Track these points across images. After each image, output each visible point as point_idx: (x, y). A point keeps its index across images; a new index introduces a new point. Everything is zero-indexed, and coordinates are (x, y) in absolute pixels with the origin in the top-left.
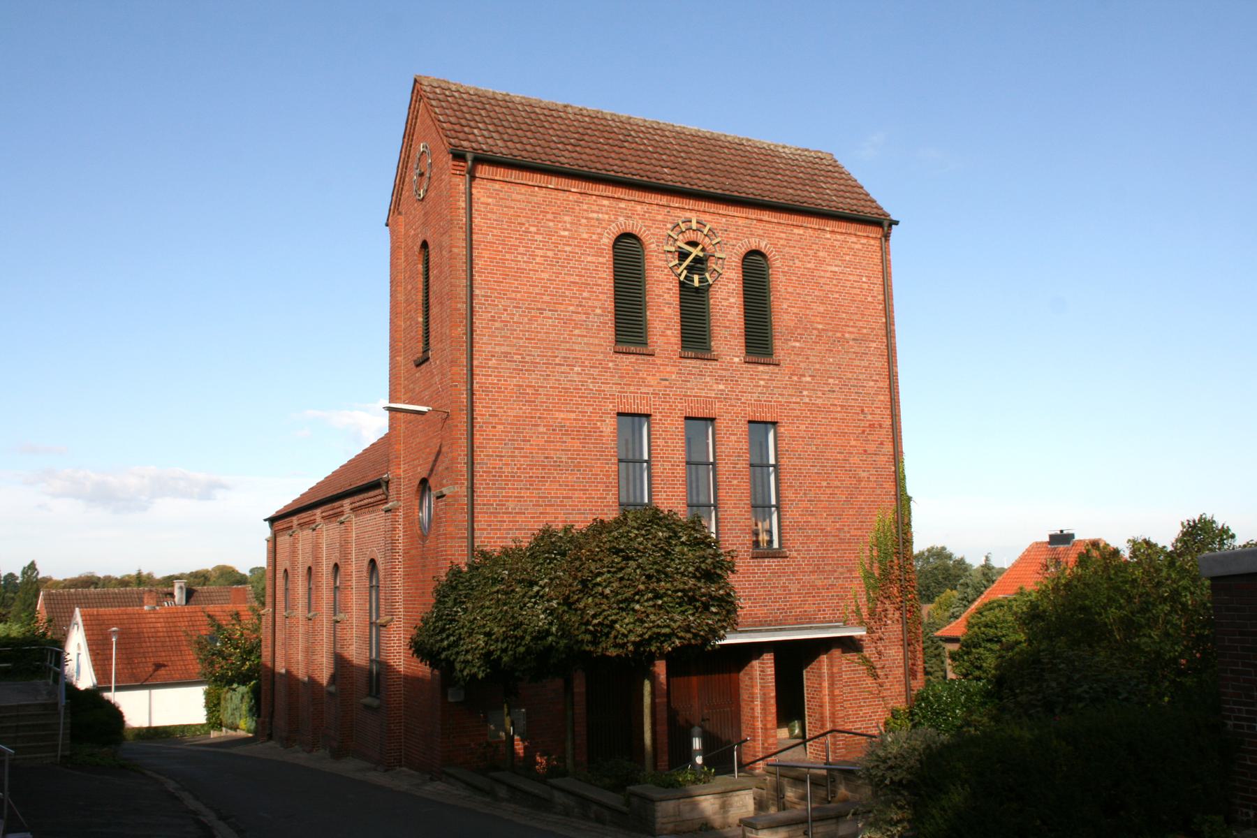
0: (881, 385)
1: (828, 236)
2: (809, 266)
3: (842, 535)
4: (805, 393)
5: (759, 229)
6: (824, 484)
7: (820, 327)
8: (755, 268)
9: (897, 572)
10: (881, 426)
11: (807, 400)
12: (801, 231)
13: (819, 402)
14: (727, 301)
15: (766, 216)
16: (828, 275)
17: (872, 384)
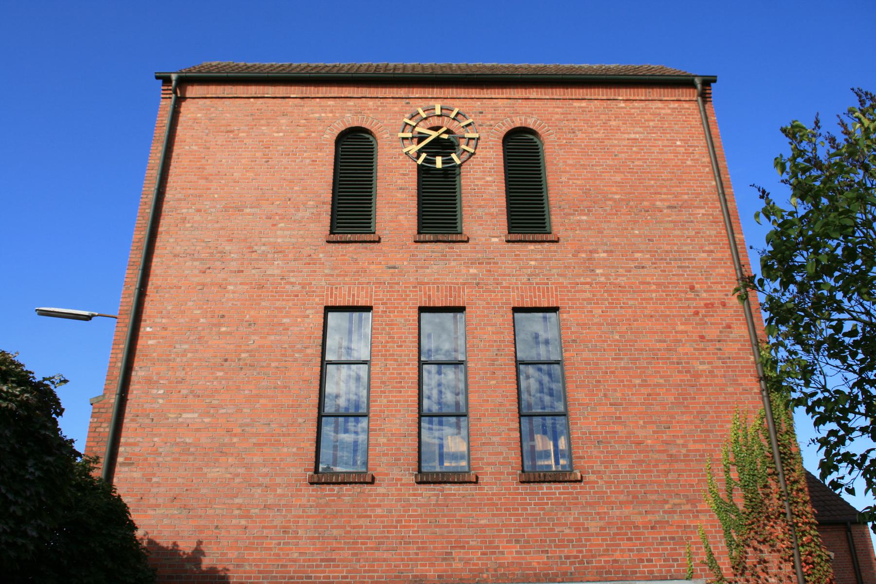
0: (719, 255)
1: (622, 105)
2: (596, 136)
3: (673, 451)
4: (598, 271)
5: (527, 106)
6: (638, 381)
7: (617, 197)
8: (522, 152)
9: (776, 503)
10: (724, 305)
11: (603, 279)
12: (584, 104)
13: (622, 280)
14: (483, 183)
15: (533, 93)
16: (626, 143)
17: (704, 255)
